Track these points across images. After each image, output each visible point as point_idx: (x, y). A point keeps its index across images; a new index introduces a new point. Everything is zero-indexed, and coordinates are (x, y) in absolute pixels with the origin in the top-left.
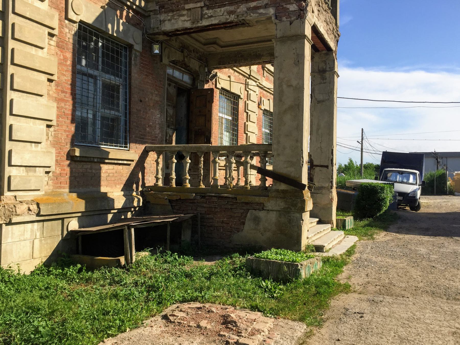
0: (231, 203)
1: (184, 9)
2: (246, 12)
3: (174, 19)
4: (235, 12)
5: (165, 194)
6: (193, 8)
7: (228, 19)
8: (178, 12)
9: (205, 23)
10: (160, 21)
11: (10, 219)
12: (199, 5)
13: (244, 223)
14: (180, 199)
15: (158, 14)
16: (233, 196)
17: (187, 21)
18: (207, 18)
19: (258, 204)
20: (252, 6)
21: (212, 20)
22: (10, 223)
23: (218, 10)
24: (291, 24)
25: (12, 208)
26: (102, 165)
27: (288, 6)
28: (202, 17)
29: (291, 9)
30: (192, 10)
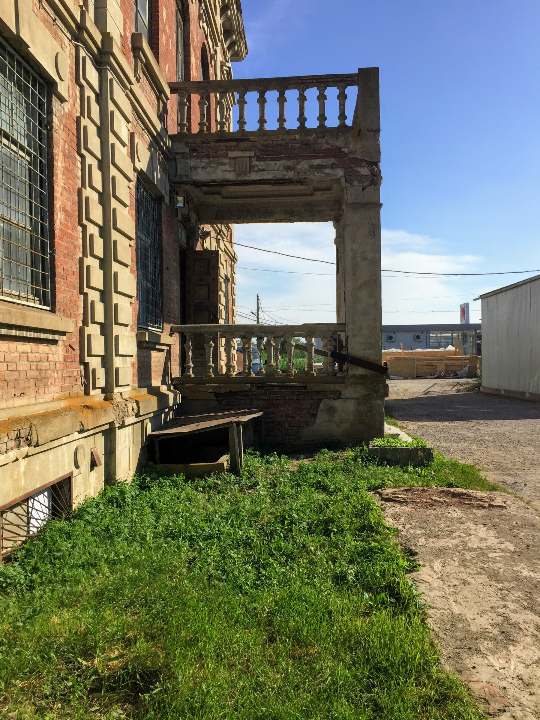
0: (297, 393)
1: (226, 156)
2: (309, 170)
3: (210, 167)
4: (295, 168)
5: (208, 386)
6: (238, 157)
7: (286, 176)
8: (216, 159)
9: (254, 176)
10: (191, 168)
11: (123, 421)
12: (247, 154)
13: (315, 416)
14: (230, 392)
15: (187, 159)
16: (302, 385)
17: (230, 171)
18: (257, 171)
19: (332, 392)
20: (315, 164)
21: (263, 175)
22: (123, 426)
23: (272, 163)
24: (363, 190)
25: (124, 408)
26: (152, 352)
27: (359, 169)
28: (252, 168)
29: (362, 173)
30: (237, 159)
